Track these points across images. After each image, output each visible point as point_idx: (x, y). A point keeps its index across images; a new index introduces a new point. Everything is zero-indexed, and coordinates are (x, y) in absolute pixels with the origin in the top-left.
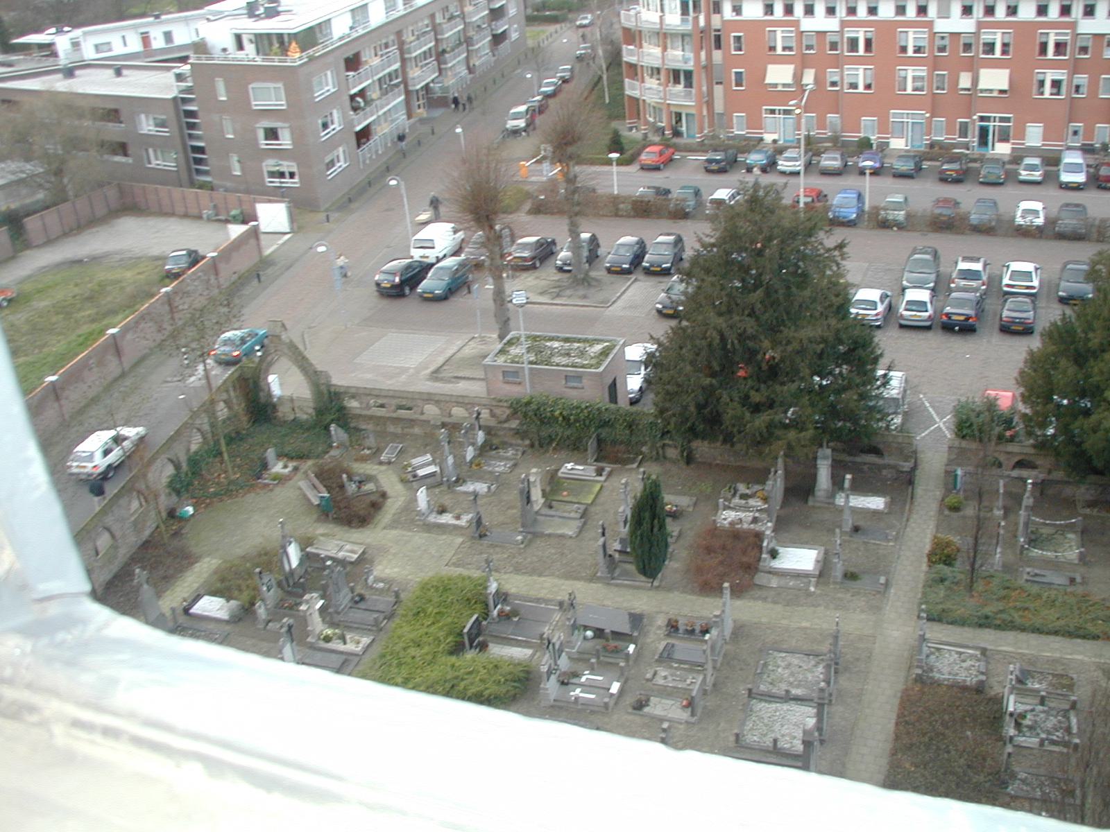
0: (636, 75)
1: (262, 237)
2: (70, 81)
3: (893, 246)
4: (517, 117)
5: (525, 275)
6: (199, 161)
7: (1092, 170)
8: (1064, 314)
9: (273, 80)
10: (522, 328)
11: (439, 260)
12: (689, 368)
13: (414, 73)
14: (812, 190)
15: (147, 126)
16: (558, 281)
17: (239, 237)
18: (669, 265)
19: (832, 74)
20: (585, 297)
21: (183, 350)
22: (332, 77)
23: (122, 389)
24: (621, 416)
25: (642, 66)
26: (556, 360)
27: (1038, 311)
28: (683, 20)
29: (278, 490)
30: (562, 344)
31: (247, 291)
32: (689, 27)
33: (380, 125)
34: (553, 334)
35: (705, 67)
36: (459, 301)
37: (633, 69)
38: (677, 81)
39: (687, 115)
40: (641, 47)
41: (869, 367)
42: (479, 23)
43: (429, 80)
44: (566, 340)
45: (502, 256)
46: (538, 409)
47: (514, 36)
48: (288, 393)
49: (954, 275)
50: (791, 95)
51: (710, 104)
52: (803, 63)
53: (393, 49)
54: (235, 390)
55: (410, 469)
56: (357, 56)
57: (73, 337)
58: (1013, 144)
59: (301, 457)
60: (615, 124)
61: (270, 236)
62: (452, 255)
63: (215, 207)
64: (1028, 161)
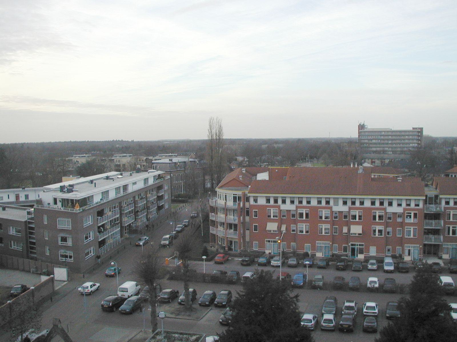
0: (215, 225)
1: (55, 282)
3: (319, 297)
5: (165, 305)
6: (32, 248)
7: (396, 265)
8: (389, 324)
9: (68, 217)
11: (129, 297)
13: (125, 219)
14: (285, 273)
15: (12, 231)
18: (225, 303)
19: (293, 227)
20: (189, 316)
21: (14, 329)
27: (378, 323)
28: (234, 204)
30: (179, 335)
34: (176, 331)
35: (242, 223)
37: (214, 223)
39: (234, 242)
40: (217, 214)
42: (152, 201)
43: (131, 222)
44: (181, 334)
45: (156, 297)
47: (166, 207)
49: (343, 308)
50: (276, 235)
51: (244, 237)
52: (281, 223)
53: (117, 209)
56: (102, 211)
58: (365, 255)
60: (205, 244)
61: (59, 282)
63: (36, 268)
64: (371, 261)
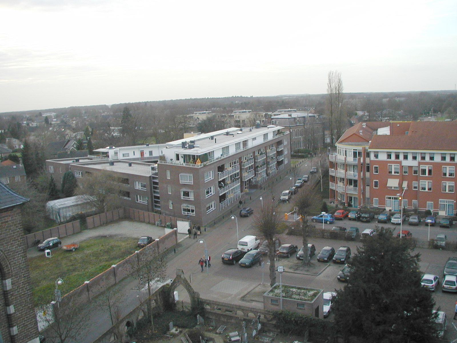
1: (178, 235)
2: (112, 167)
4: (285, 195)
5: (283, 260)
10: (281, 282)
11: (248, 251)
12: (350, 304)
13: (245, 174)
14: (406, 231)
15: (138, 186)
16: (297, 263)
17: (169, 234)
18: (344, 260)
19: (415, 184)
20: (308, 271)
22: (212, 173)
23: (114, 290)
24: (320, 322)
25: (337, 177)
26: (294, 296)
29: (172, 340)
30: (297, 290)
31: (169, 256)
32: (356, 162)
33: (229, 194)
35: (362, 179)
36: (256, 268)
37: (333, 179)
38: (351, 184)
39: (354, 198)
40: (337, 169)
41: (429, 309)
42: (272, 156)
44: (299, 288)
45: (275, 251)
46: (285, 317)
47: (286, 162)
48: (181, 300)
50: (398, 192)
51: (364, 194)
52: (402, 179)
53: (238, 164)
54: (160, 295)
55: (228, 337)
56: (223, 166)
57: (98, 266)
59: (183, 327)
60: (324, 200)
62: (254, 249)
63: (161, 221)
